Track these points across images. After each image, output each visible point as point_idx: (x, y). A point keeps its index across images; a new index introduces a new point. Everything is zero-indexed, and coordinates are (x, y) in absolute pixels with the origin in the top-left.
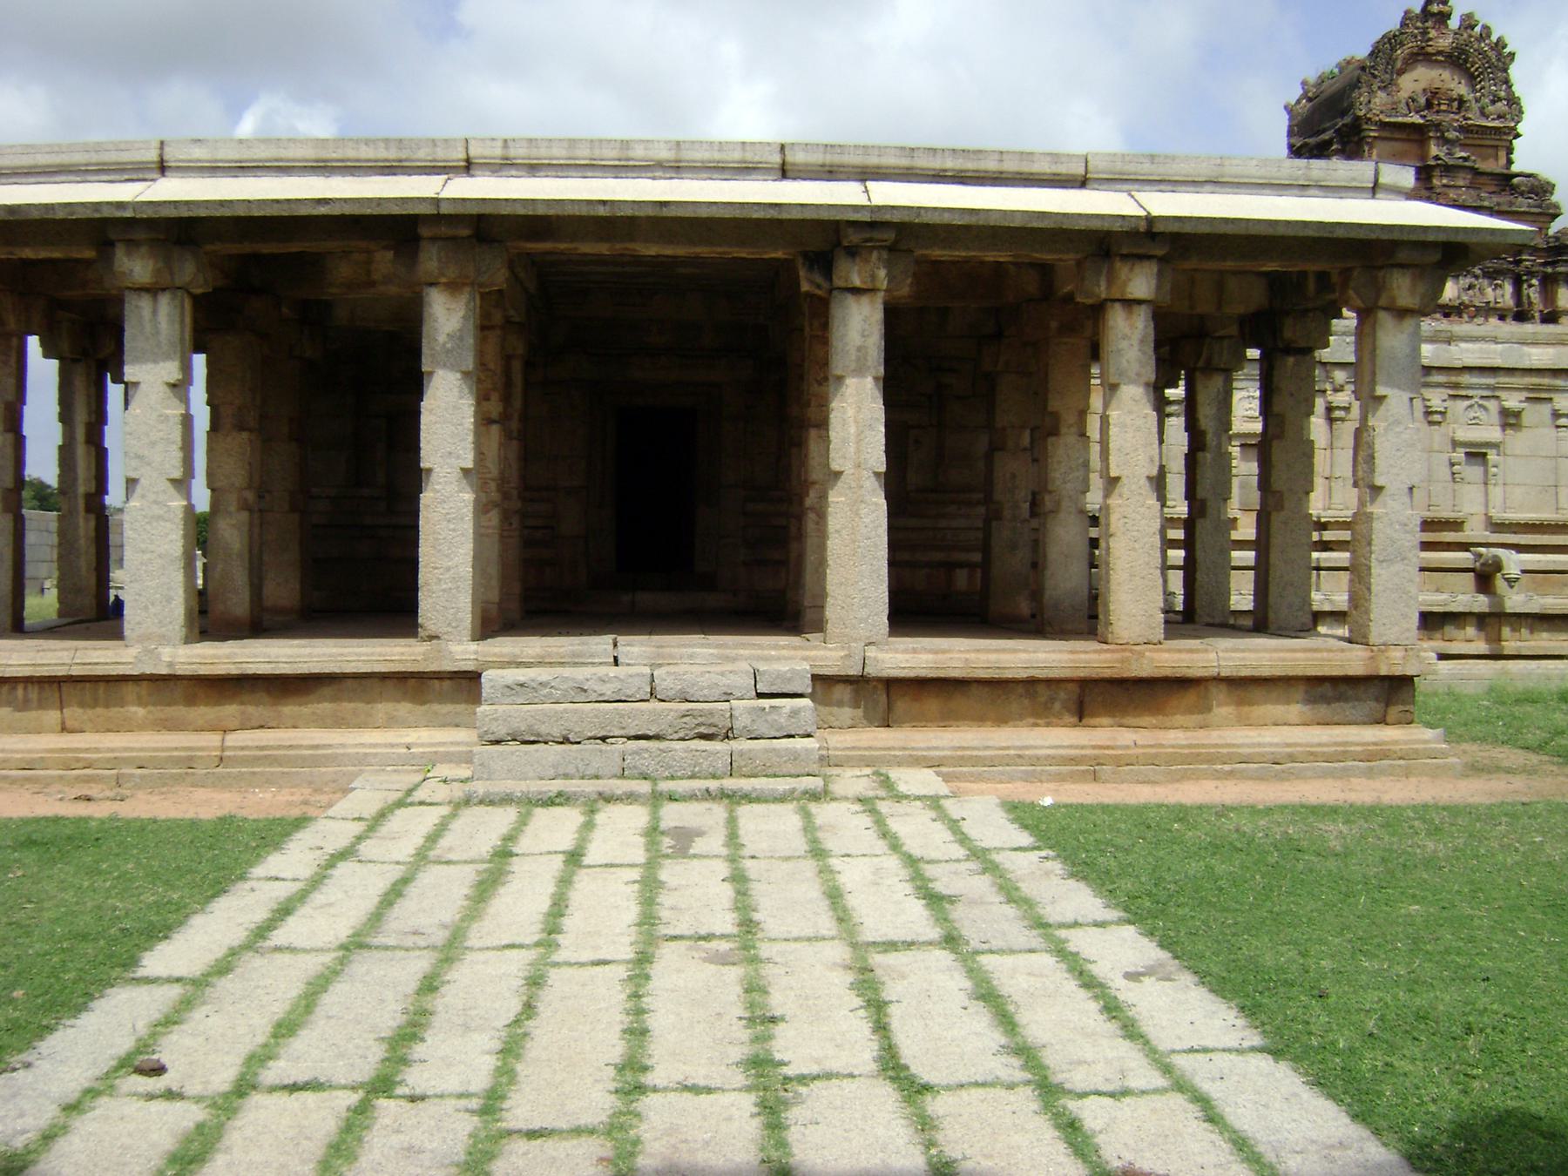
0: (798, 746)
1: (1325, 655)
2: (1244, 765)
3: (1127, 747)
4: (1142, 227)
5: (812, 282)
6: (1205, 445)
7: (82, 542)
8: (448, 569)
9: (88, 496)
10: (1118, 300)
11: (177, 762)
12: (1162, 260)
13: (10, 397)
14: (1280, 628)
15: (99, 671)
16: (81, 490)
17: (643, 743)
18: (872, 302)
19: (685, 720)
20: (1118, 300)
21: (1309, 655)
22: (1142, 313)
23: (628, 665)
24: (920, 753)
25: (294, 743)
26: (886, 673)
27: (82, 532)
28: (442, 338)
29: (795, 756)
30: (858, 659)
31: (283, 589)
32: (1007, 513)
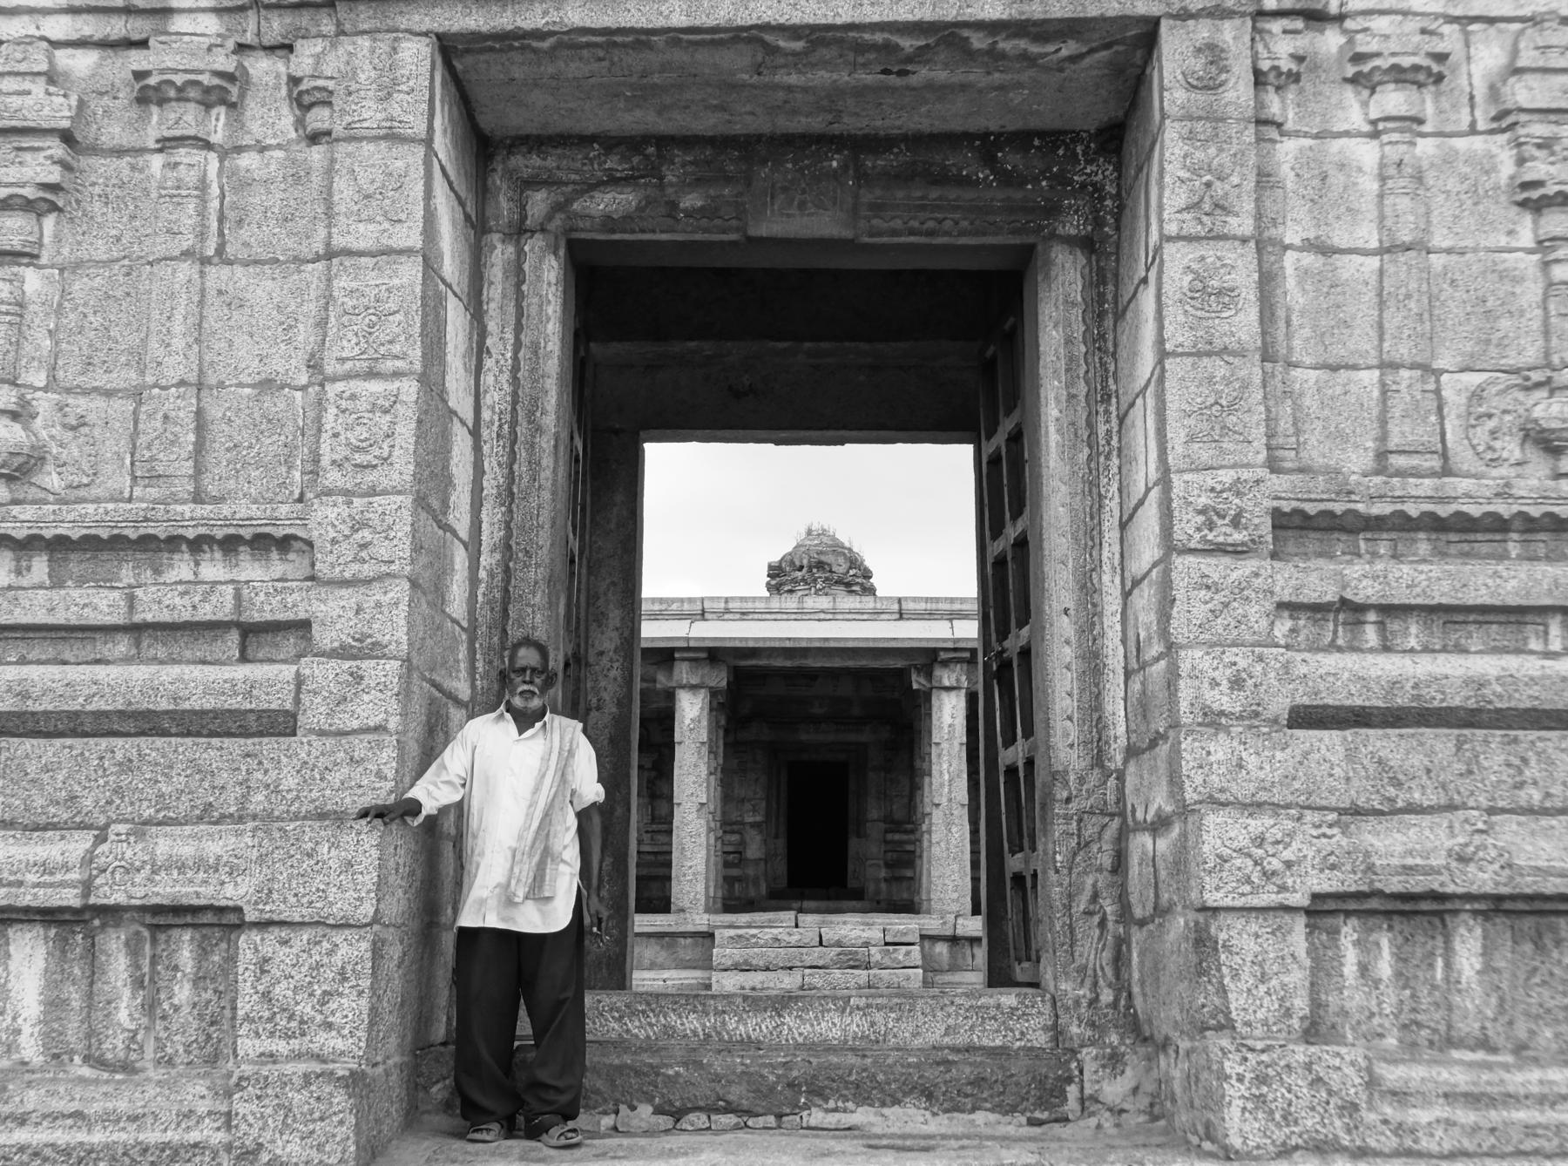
28: (687, 722)
30: (950, 925)
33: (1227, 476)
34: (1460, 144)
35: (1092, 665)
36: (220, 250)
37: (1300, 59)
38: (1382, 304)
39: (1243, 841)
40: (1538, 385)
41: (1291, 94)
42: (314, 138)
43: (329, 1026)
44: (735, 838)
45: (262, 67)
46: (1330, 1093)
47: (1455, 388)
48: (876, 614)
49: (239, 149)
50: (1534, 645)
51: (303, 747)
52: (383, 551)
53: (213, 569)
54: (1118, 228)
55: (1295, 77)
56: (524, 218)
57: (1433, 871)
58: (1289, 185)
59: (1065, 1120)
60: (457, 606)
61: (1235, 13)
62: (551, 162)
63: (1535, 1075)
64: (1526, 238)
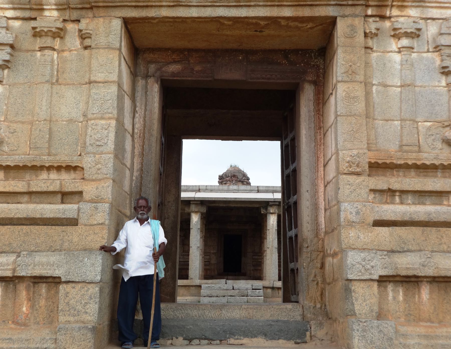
18: (275, 215)
28: (194, 222)
33: (355, 152)
34: (425, 55)
35: (316, 207)
36: (57, 81)
37: (378, 29)
38: (401, 101)
39: (359, 260)
40: (447, 126)
41: (375, 40)
42: (86, 48)
43: (86, 313)
44: (208, 257)
45: (70, 27)
46: (384, 335)
47: (424, 126)
48: (251, 191)
49: (63, 51)
50: (445, 203)
51: (79, 229)
52: (104, 171)
53: (53, 175)
54: (324, 78)
55: (376, 35)
56: (148, 72)
57: (416, 269)
58: (374, 66)
59: (306, 342)
60: (127, 188)
61: (359, 15)
62: (156, 56)
63: (445, 330)
64: (444, 83)
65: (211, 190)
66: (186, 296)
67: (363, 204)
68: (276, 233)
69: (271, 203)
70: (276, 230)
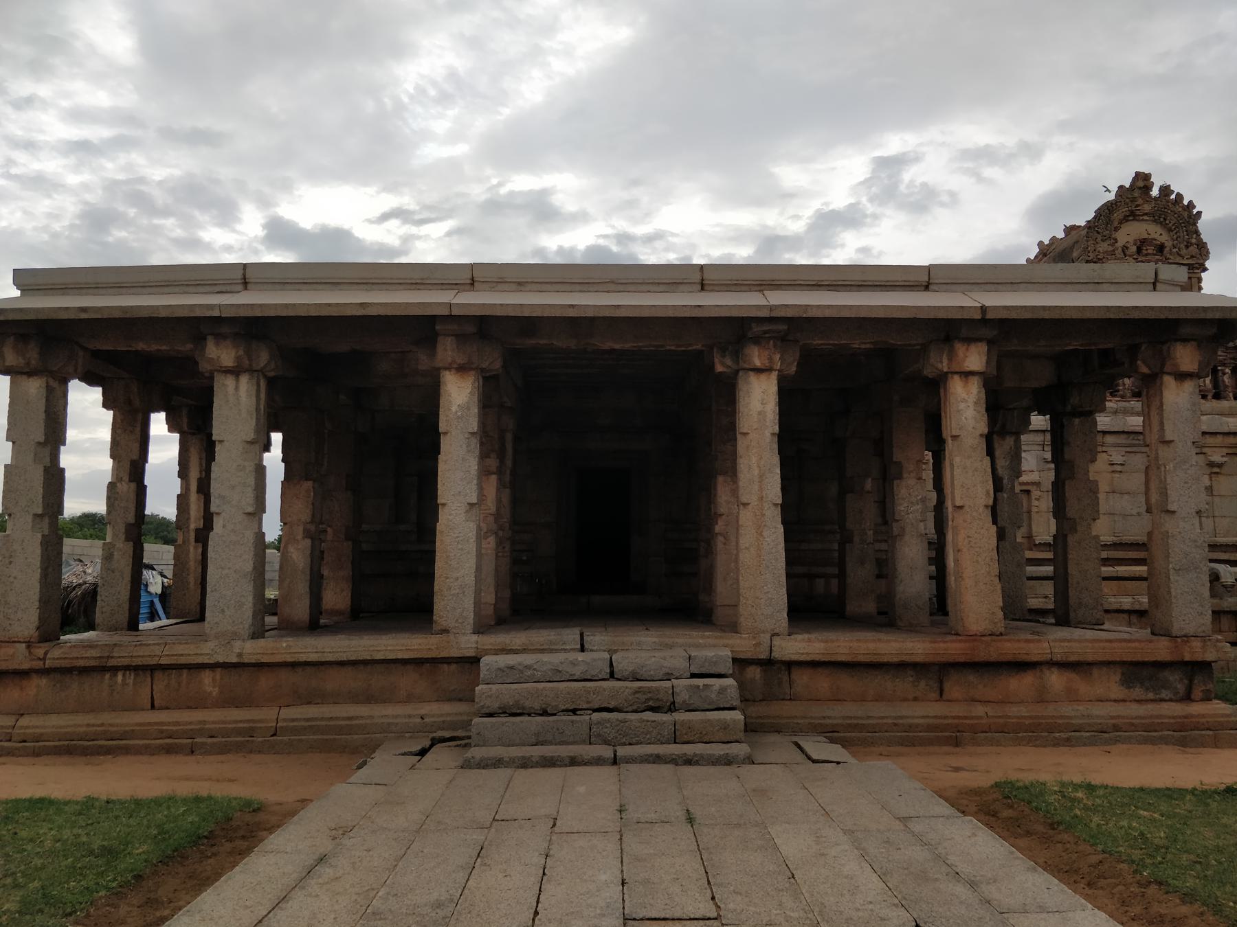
0: (728, 718)
1: (1137, 644)
2: (1078, 734)
3: (981, 718)
4: (978, 316)
5: (723, 364)
6: (1002, 488)
7: (192, 563)
8: (457, 579)
9: (197, 530)
10: (956, 373)
11: (239, 732)
12: (990, 343)
13: (135, 457)
14: (1080, 622)
15: (183, 661)
16: (192, 526)
17: (605, 715)
19: (637, 696)
20: (956, 373)
21: (1124, 644)
22: (976, 382)
23: (592, 650)
24: (817, 721)
25: (334, 715)
26: (786, 658)
27: (192, 555)
28: (454, 409)
29: (725, 726)
31: (336, 597)
32: (856, 539)
65: (519, 283)
66: (421, 700)
67: (968, 398)
68: (776, 446)
69: (757, 329)
70: (773, 434)
